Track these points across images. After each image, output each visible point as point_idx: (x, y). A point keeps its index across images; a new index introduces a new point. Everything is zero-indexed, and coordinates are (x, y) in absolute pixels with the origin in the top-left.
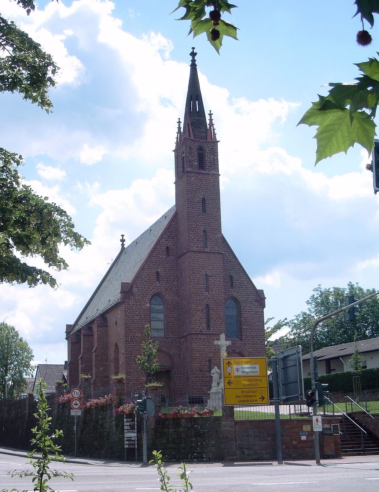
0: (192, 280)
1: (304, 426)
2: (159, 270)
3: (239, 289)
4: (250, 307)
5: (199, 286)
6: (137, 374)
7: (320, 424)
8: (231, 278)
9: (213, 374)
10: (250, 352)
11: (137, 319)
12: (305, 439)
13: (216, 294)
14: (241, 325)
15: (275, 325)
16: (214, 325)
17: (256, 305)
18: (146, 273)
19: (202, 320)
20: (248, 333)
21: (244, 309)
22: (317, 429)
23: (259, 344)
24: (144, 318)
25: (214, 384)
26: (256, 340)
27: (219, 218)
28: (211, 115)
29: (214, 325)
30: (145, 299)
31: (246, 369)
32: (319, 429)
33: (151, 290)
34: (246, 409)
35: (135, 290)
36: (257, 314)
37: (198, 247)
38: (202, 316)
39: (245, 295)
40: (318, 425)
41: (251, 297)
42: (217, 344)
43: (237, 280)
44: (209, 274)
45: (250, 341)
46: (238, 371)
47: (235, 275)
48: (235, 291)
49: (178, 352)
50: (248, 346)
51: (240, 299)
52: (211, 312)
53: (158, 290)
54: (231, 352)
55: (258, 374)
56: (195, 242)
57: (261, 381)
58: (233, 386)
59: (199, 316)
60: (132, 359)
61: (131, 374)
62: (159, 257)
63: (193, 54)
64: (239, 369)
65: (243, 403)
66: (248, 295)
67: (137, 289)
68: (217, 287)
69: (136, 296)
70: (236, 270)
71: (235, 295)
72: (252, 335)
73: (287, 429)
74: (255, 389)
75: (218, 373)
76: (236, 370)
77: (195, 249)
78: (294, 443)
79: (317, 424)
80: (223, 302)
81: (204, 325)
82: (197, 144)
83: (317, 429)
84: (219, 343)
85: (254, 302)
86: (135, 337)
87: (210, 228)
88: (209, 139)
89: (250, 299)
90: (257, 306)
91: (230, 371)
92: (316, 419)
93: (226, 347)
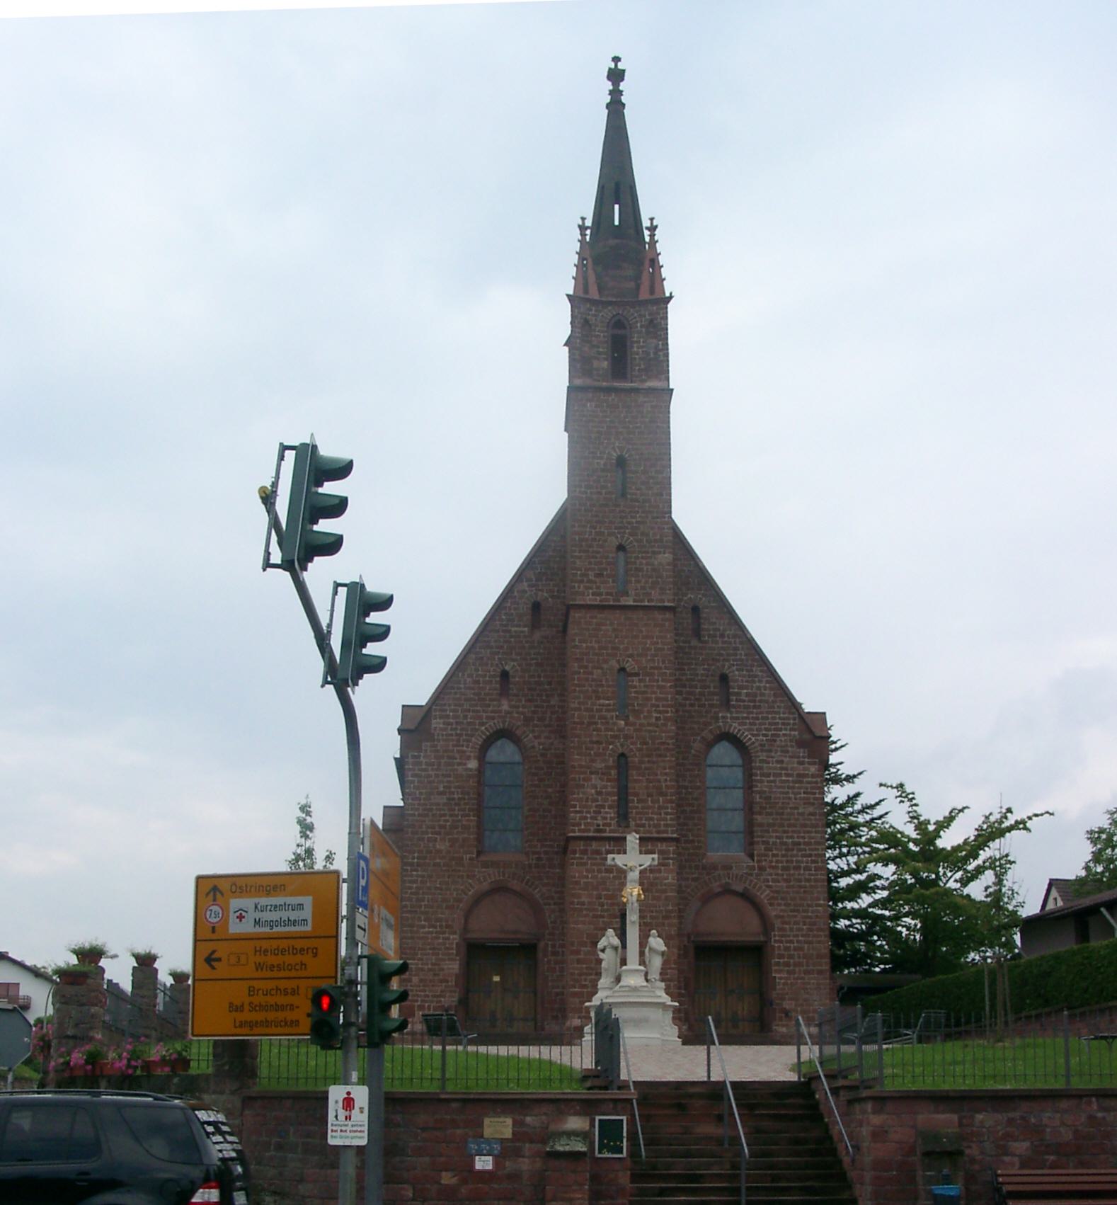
0: (579, 686)
1: (487, 1121)
2: (507, 668)
3: (749, 713)
4: (782, 762)
5: (598, 702)
6: (433, 954)
7: (361, 1117)
8: (724, 678)
9: (603, 951)
10: (777, 892)
11: (438, 804)
12: (490, 1167)
13: (649, 725)
14: (753, 814)
15: (977, 827)
16: (640, 813)
17: (799, 757)
18: (470, 676)
19: (606, 800)
20: (771, 837)
21: (761, 768)
22: (347, 1137)
23: (807, 868)
24: (459, 799)
25: (604, 982)
26: (797, 856)
27: (666, 510)
28: (653, 229)
29: (640, 813)
30: (465, 748)
31: (270, 910)
32: (352, 1138)
33: (482, 724)
34: (523, 1051)
35: (437, 723)
36: (801, 782)
37: (600, 594)
38: (606, 787)
39: (766, 730)
40: (350, 1123)
41: (784, 735)
42: (613, 863)
43: (741, 687)
44: (630, 665)
45: (434, 828)
46: (241, 918)
47: (737, 673)
48: (737, 718)
49: (556, 892)
50: (771, 875)
51: (750, 739)
52: (634, 774)
53: (504, 722)
54: (719, 890)
55: (308, 928)
56: (591, 581)
57: (315, 955)
58: (222, 969)
59: (595, 787)
60: (422, 913)
61: (417, 954)
62: (509, 631)
63: (616, 76)
64: (247, 912)
65: (252, 1033)
66: (775, 730)
67: (442, 721)
68: (653, 706)
69: (439, 740)
70: (741, 660)
71: (735, 728)
72: (786, 844)
73: (424, 1129)
74: (293, 984)
75: (616, 948)
76: (238, 914)
77: (589, 599)
78: (447, 1179)
79: (348, 1118)
80: (671, 746)
81: (611, 814)
82: (608, 313)
83: (347, 1137)
84: (620, 860)
85: (792, 746)
86: (431, 852)
87: (637, 541)
88: (644, 295)
89: (783, 739)
90: (804, 757)
91: (218, 919)
92: (345, 1099)
93: (641, 872)
